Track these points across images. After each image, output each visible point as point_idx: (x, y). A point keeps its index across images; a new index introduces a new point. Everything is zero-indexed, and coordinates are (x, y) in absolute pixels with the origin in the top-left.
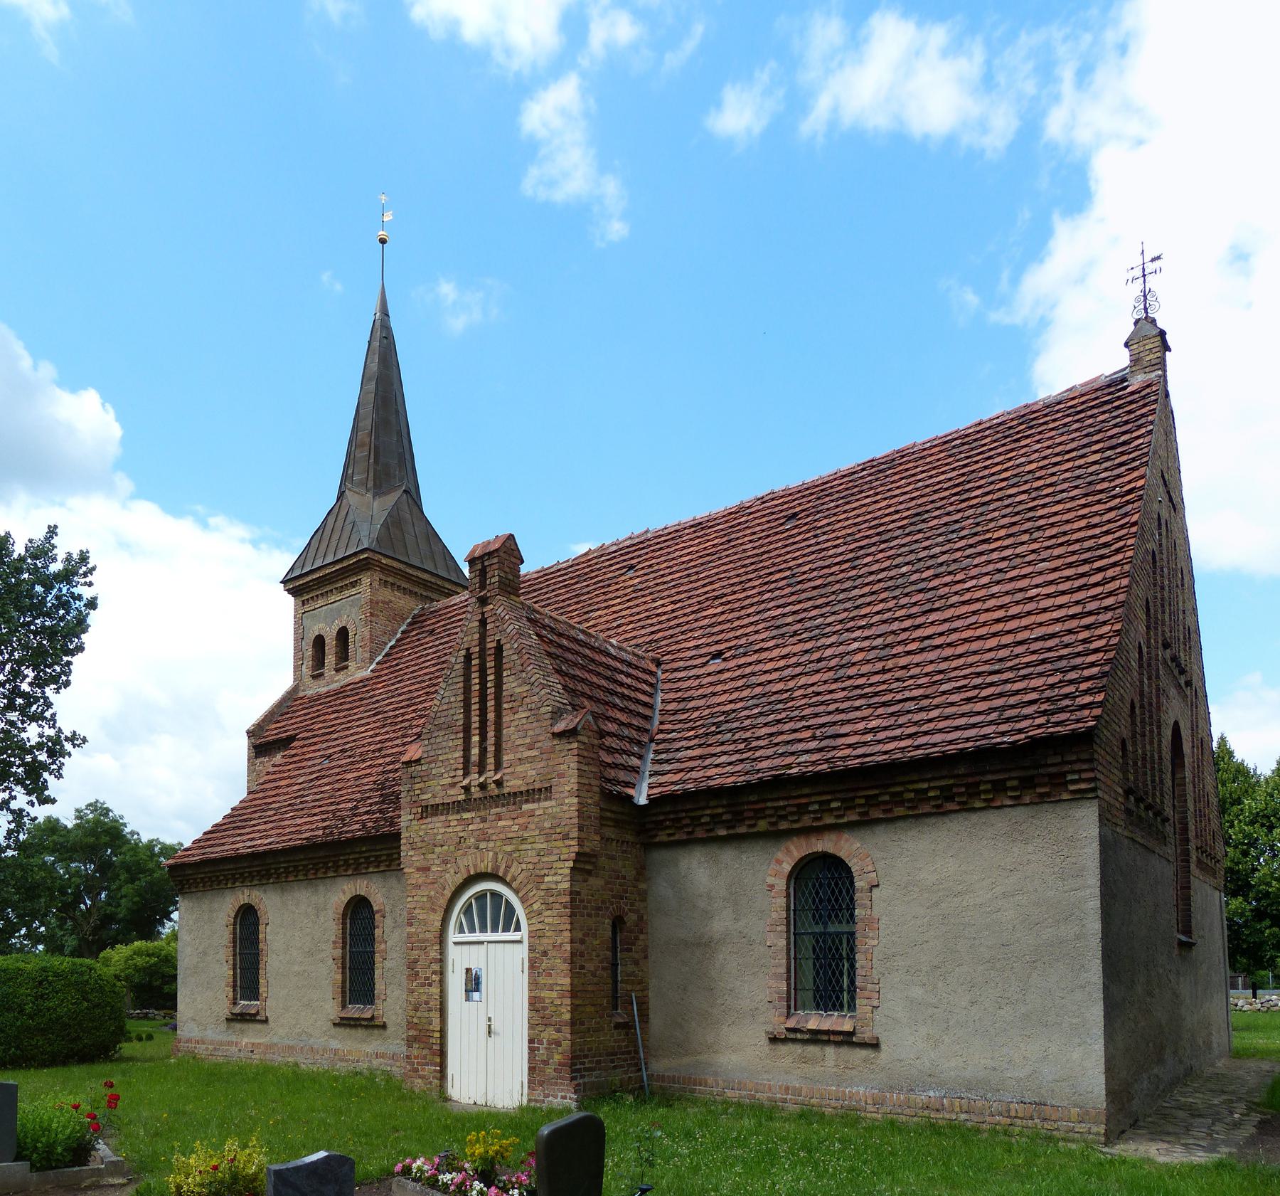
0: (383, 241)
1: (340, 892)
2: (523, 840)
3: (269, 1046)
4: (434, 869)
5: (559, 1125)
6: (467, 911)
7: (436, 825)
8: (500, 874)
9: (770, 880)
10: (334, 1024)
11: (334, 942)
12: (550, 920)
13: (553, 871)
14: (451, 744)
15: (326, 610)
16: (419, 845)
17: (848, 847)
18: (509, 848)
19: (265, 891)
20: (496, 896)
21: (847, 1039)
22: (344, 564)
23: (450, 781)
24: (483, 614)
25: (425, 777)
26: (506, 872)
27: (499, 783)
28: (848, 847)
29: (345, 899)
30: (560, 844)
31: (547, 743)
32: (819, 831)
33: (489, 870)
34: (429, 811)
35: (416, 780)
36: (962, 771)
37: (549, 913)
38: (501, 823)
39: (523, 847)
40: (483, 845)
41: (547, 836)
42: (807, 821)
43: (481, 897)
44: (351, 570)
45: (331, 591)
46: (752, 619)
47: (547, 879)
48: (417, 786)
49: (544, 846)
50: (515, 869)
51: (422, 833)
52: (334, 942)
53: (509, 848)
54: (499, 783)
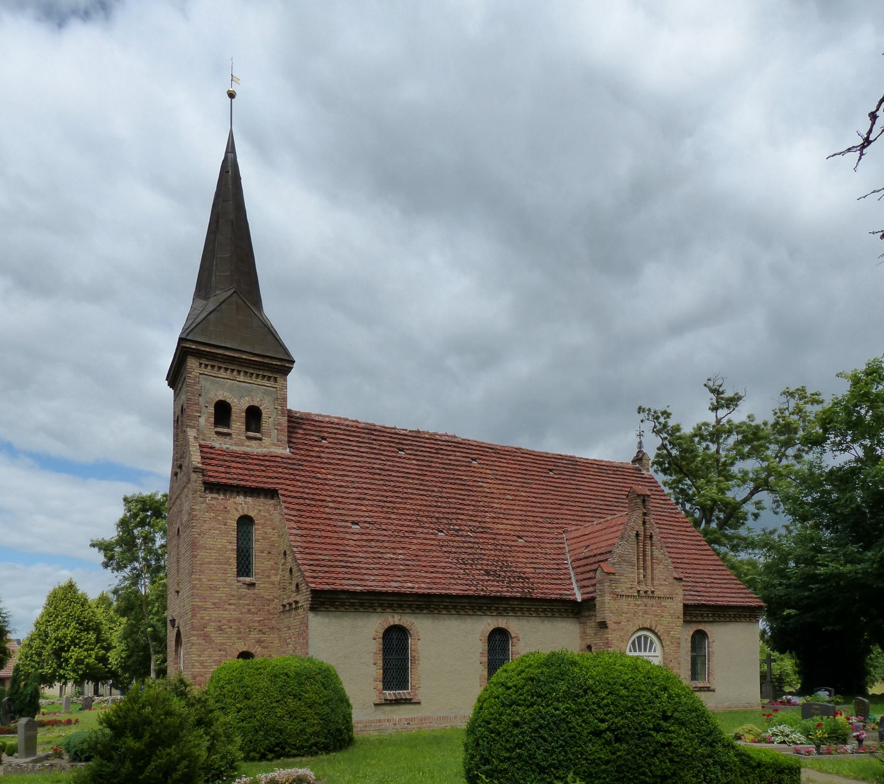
0: (232, 95)
1: (486, 624)
2: (662, 617)
3: (422, 720)
4: (623, 623)
5: (286, 766)
6: (633, 643)
7: (623, 603)
8: (653, 629)
9: (686, 637)
10: (376, 705)
11: (481, 653)
12: (673, 648)
13: (673, 630)
14: (630, 570)
15: (233, 384)
16: (615, 611)
17: (707, 628)
18: (657, 619)
19: (416, 618)
20: (646, 638)
21: (408, 701)
22: (266, 361)
23: (630, 586)
24: (644, 519)
25: (617, 581)
26: (655, 628)
27: (653, 592)
28: (707, 628)
29: (490, 629)
30: (676, 620)
31: (671, 580)
32: (700, 622)
33: (649, 627)
34: (618, 596)
35: (613, 582)
36: (740, 611)
37: (672, 646)
38: (653, 608)
39: (662, 619)
40: (645, 616)
41: (672, 616)
42: (700, 619)
43: (639, 638)
44: (268, 367)
45: (252, 374)
46: (307, 474)
47: (671, 633)
48: (613, 585)
49: (671, 620)
50: (659, 627)
51: (616, 607)
52: (481, 653)
53: (657, 619)
54: (653, 592)
